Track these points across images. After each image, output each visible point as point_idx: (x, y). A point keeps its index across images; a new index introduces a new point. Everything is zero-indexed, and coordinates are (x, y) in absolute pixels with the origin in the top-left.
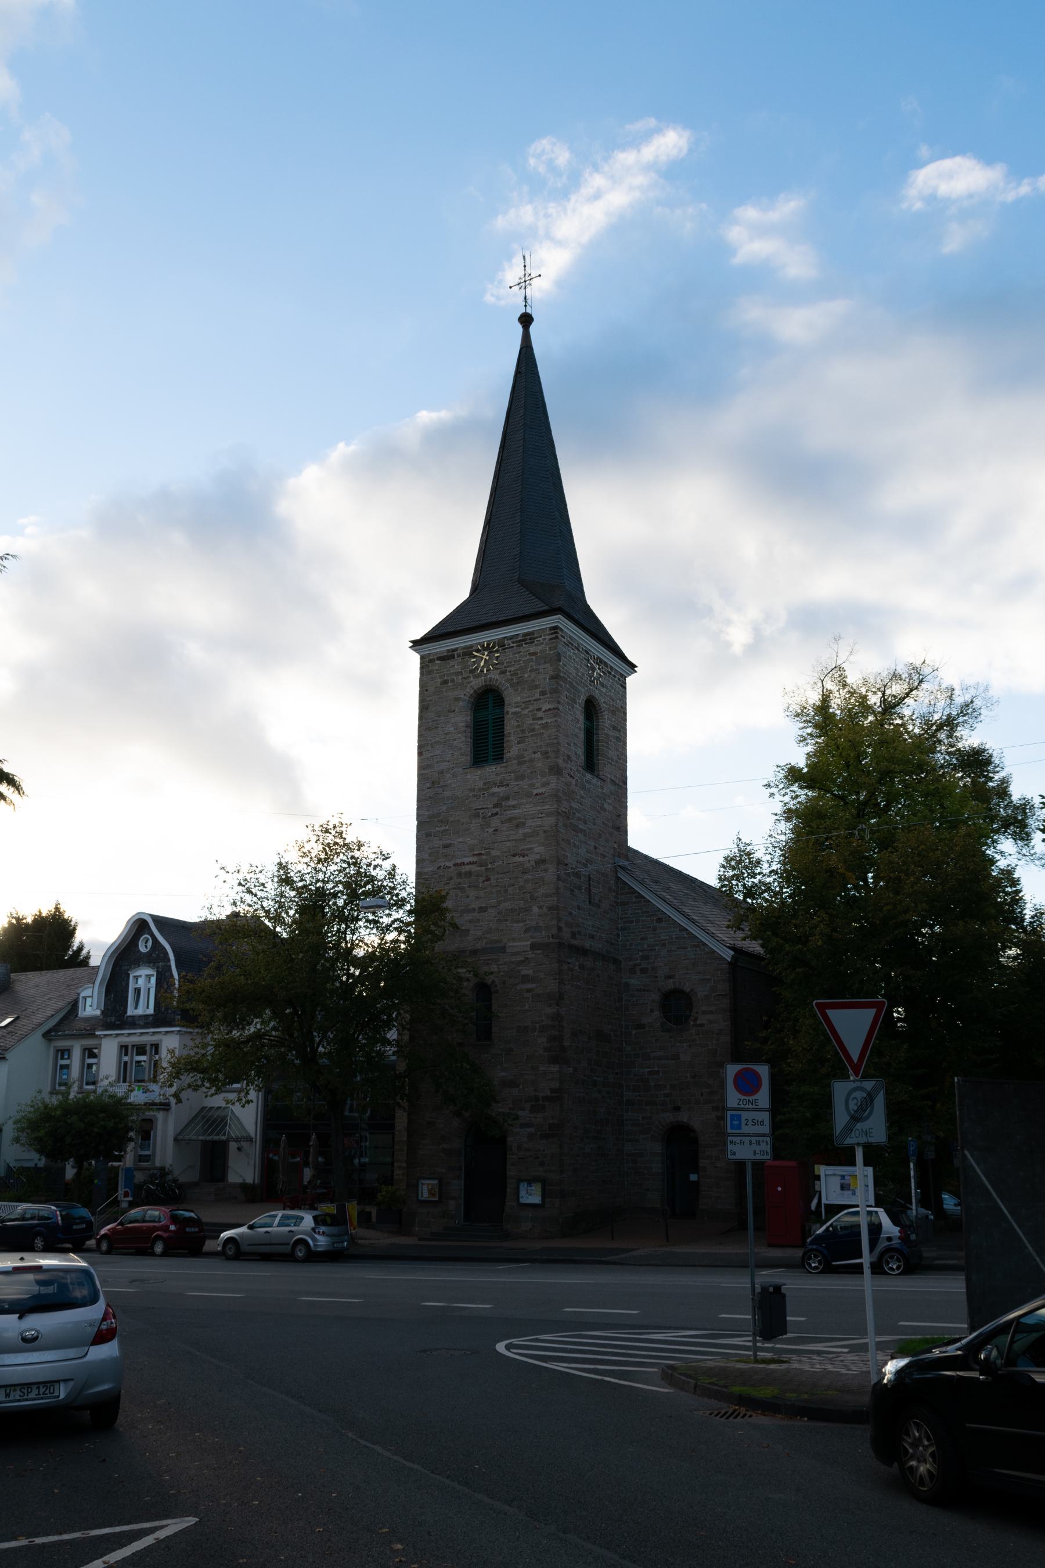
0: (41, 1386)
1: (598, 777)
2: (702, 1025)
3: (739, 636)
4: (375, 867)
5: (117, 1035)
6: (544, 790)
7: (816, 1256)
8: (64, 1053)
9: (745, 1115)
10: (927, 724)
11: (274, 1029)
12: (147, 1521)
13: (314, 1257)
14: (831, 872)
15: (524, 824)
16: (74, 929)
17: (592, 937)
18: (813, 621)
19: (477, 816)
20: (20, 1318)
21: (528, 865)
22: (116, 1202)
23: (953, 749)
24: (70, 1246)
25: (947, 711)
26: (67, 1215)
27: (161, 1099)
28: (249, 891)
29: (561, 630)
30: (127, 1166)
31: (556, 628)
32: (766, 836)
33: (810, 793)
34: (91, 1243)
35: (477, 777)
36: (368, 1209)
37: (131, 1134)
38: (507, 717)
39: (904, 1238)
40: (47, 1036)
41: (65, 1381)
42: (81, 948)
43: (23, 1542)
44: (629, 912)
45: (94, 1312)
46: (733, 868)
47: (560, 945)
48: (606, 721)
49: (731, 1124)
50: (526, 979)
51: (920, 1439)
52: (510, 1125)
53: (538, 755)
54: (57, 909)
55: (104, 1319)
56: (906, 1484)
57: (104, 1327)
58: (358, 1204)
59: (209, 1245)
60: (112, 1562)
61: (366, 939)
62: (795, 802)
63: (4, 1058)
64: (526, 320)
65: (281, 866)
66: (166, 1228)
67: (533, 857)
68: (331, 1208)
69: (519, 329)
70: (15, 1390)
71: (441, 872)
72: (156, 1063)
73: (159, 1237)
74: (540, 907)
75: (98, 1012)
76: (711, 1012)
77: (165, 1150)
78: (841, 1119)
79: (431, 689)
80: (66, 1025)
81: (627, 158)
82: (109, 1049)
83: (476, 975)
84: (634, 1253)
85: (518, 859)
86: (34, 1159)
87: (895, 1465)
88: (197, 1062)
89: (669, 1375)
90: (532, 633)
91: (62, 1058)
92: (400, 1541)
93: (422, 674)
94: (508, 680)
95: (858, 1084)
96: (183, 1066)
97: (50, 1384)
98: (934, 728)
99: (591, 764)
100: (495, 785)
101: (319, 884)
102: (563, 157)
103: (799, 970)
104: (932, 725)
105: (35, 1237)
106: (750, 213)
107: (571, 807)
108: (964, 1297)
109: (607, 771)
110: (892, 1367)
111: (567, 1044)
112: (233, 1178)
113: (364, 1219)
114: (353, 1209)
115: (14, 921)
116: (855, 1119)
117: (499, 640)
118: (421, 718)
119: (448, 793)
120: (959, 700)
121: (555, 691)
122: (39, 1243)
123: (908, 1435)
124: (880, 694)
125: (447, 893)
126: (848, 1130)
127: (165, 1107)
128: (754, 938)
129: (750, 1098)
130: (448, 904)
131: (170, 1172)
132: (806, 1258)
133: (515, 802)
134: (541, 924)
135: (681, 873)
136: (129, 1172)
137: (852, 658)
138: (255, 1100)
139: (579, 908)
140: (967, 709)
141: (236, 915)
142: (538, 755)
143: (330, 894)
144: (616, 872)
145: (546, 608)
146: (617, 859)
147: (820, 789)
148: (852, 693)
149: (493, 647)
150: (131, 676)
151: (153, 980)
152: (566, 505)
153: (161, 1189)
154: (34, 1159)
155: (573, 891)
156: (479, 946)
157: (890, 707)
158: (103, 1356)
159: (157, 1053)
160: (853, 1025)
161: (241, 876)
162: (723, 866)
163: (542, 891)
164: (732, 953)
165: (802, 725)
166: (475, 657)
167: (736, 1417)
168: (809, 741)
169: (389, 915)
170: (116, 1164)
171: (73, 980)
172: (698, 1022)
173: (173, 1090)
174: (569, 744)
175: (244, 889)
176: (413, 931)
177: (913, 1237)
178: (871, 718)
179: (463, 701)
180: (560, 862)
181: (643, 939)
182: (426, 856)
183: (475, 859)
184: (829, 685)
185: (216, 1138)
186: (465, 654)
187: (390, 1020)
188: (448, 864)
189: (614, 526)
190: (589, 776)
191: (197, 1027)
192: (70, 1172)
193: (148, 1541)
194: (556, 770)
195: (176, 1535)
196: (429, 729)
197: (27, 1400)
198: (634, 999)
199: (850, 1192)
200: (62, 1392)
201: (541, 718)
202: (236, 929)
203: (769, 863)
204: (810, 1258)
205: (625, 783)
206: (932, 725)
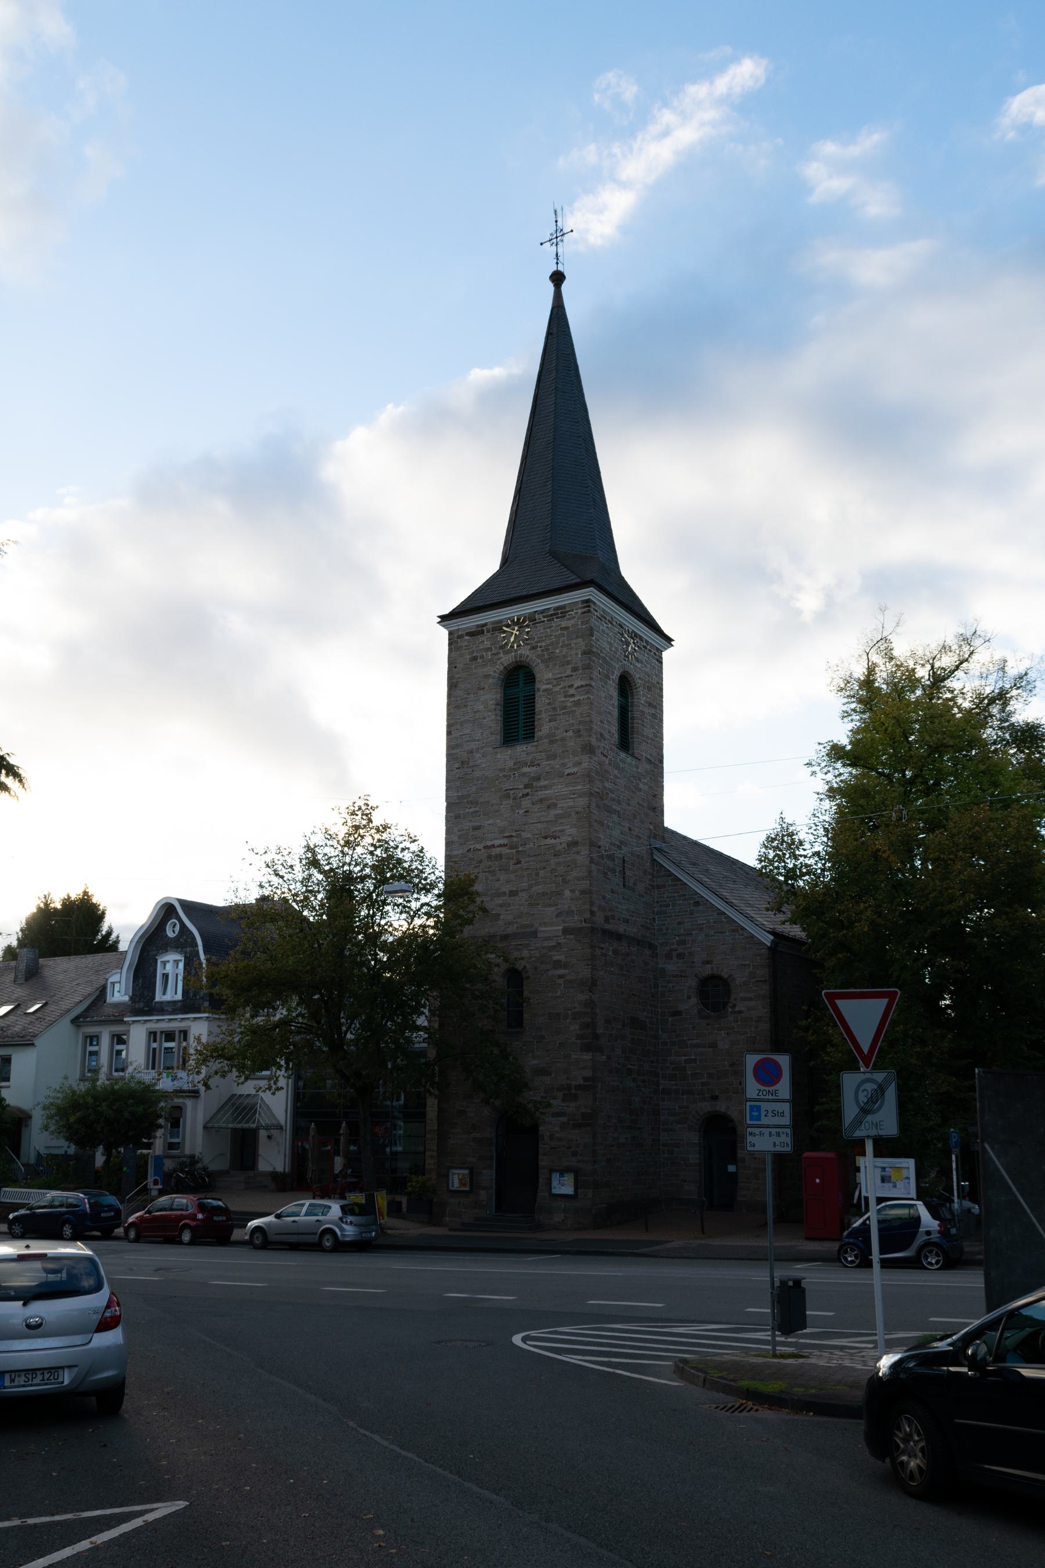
0: (46, 1372)
1: (633, 755)
2: (741, 1012)
3: (809, 603)
4: (403, 850)
6: (575, 770)
7: (852, 1250)
8: (93, 1039)
9: (764, 1106)
10: (980, 698)
11: (300, 1015)
12: (138, 1504)
13: (341, 1247)
14: (876, 855)
15: (555, 805)
16: (103, 913)
17: (627, 921)
18: (888, 586)
19: (508, 797)
20: (24, 1305)
22: (145, 1190)
23: (1007, 724)
24: (98, 1234)
25: (1000, 684)
26: (96, 1202)
27: (190, 1087)
29: (594, 603)
30: (157, 1153)
31: (588, 601)
32: (810, 815)
33: (854, 772)
34: (119, 1231)
35: (506, 757)
36: (398, 1198)
37: (161, 1121)
39: (944, 1232)
40: (75, 1021)
41: (70, 1367)
42: (109, 933)
43: (16, 1522)
44: (666, 895)
45: (99, 1300)
46: (776, 848)
47: (593, 930)
48: (641, 697)
49: (751, 1115)
50: (558, 965)
51: (910, 1435)
52: (542, 1113)
53: (570, 733)
54: (85, 893)
55: (108, 1307)
56: (897, 1479)
57: (108, 1314)
59: (237, 1234)
60: (99, 1542)
61: (396, 922)
62: (838, 779)
63: (33, 1044)
64: (558, 278)
65: (308, 848)
66: (193, 1217)
67: (565, 839)
68: (359, 1198)
69: (551, 288)
70: (19, 1376)
71: (470, 855)
72: (185, 1048)
73: (186, 1226)
74: (573, 891)
75: (126, 998)
76: (750, 999)
77: (194, 1138)
78: (850, 1111)
79: (460, 666)
80: (94, 1011)
81: (698, 91)
82: (138, 1035)
83: (506, 960)
84: (668, 1246)
85: (549, 841)
86: (63, 1146)
87: (888, 1460)
88: (223, 1049)
89: (682, 1369)
90: (564, 607)
91: (91, 1044)
92: (383, 1527)
93: (450, 650)
94: (539, 656)
95: (868, 1076)
96: (213, 1052)
97: (54, 1370)
98: (986, 701)
99: (625, 743)
100: (526, 764)
101: (346, 868)
102: (630, 91)
103: (840, 956)
104: (984, 699)
105: (63, 1225)
106: (829, 148)
107: (605, 787)
108: (983, 1293)
109: (642, 749)
110: (886, 1362)
111: (600, 1031)
112: (263, 1166)
113: (395, 1210)
114: (382, 1200)
115: (42, 905)
116: (865, 1111)
117: (531, 613)
118: (450, 696)
119: (477, 774)
120: (1013, 671)
121: (588, 667)
122: (67, 1230)
123: (900, 1431)
124: (928, 667)
125: (477, 877)
126: (858, 1122)
127: (194, 1094)
128: (793, 921)
129: (771, 1089)
130: (478, 887)
131: (200, 1160)
132: (842, 1250)
133: (546, 783)
134: (573, 908)
135: (721, 855)
136: (159, 1160)
137: (898, 630)
138: (285, 1087)
139: (612, 891)
140: (1021, 681)
141: (264, 899)
142: (570, 733)
143: (357, 878)
144: (652, 854)
146: (653, 840)
147: (864, 767)
148: (898, 666)
149: (524, 621)
150: (172, 650)
151: (181, 965)
152: (599, 473)
153: (190, 1177)
154: (63, 1146)
156: (510, 930)
157: (938, 679)
158: (108, 1343)
159: (185, 1039)
160: (863, 1016)
161: (268, 858)
162: (766, 847)
163: (574, 874)
164: (772, 937)
165: (846, 700)
166: (505, 632)
167: (741, 1412)
168: (854, 717)
169: (417, 899)
170: (145, 1151)
171: (101, 965)
172: (737, 1009)
173: (202, 1076)
174: (601, 722)
175: (270, 871)
176: (442, 915)
177: (953, 1231)
178: (919, 693)
179: (493, 677)
180: (593, 844)
181: (679, 923)
182: (455, 838)
183: (505, 841)
184: (875, 658)
185: (246, 1126)
186: (494, 629)
187: (419, 1005)
188: (478, 846)
189: (651, 496)
190: (623, 755)
191: (223, 1013)
192: (100, 1160)
193: (138, 1522)
195: (165, 1517)
196: (458, 707)
197: (31, 1385)
198: (671, 985)
199: (891, 1185)
200: (67, 1378)
201: (573, 695)
202: (266, 912)
203: (813, 845)
204: (846, 1252)
205: (661, 762)
206: (984, 699)
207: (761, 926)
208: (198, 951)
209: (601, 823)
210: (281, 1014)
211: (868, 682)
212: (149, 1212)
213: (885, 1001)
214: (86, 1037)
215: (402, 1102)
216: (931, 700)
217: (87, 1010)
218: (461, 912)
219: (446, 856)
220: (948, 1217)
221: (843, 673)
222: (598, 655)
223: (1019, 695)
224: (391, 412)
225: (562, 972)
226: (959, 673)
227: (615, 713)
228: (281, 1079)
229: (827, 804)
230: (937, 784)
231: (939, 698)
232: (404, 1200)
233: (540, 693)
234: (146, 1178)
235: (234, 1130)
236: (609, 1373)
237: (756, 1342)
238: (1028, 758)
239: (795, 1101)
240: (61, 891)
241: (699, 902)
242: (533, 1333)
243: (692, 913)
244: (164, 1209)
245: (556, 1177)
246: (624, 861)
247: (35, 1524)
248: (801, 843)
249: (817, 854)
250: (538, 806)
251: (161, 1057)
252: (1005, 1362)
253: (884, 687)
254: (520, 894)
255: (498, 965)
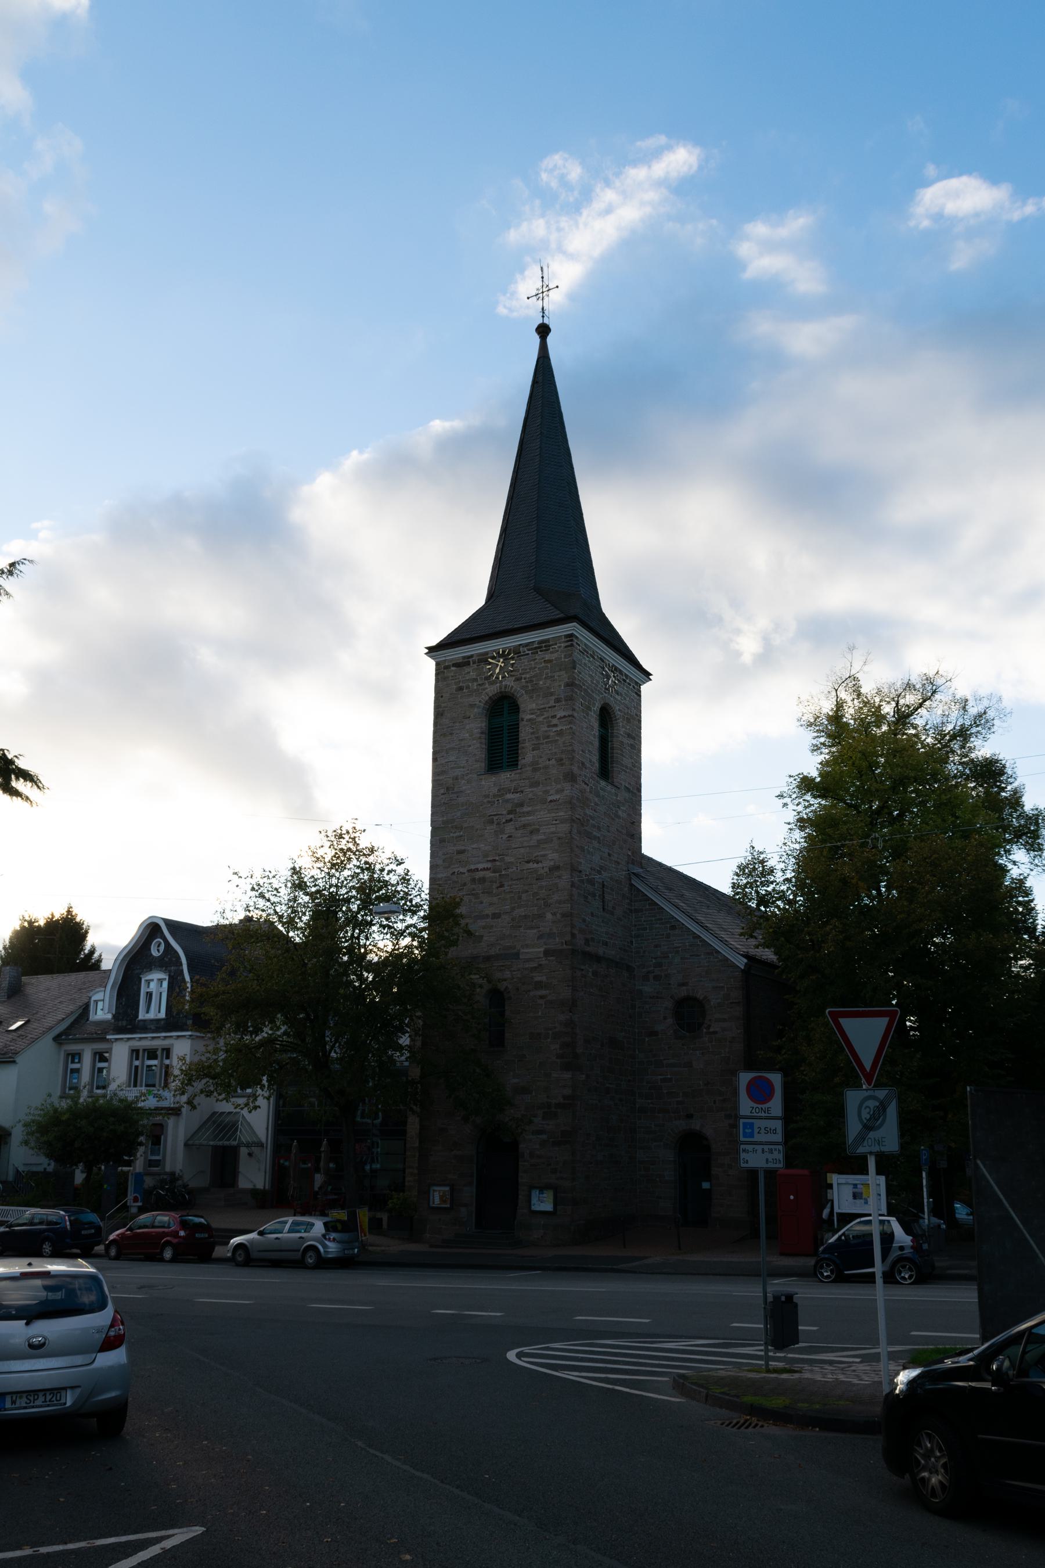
1: (612, 784)
2: (715, 1033)
3: (749, 646)
4: (389, 872)
5: (129, 1039)
6: (558, 797)
7: (828, 1265)
8: (75, 1057)
9: (757, 1123)
13: (324, 1263)
15: (538, 830)
16: (87, 932)
17: (606, 944)
19: (492, 822)
20: (27, 1324)
21: (542, 871)
22: (125, 1207)
24: (78, 1251)
26: (76, 1220)
28: (262, 896)
30: (137, 1170)
31: (571, 635)
32: (781, 844)
33: (823, 802)
34: (100, 1248)
35: (491, 783)
36: (379, 1215)
37: (142, 1139)
38: (521, 724)
39: (916, 1248)
40: (57, 1039)
41: (72, 1388)
42: (92, 952)
43: (27, 1551)
45: (102, 1319)
48: (621, 728)
49: (744, 1132)
50: (539, 985)
51: (932, 1450)
53: (553, 762)
54: (69, 912)
55: (112, 1326)
56: (917, 1495)
57: (112, 1334)
58: (370, 1210)
59: (219, 1251)
61: (380, 943)
62: (808, 810)
64: (543, 330)
65: (295, 871)
66: (175, 1234)
68: (341, 1215)
69: (537, 339)
70: (21, 1397)
73: (168, 1243)
74: (554, 914)
75: (109, 1016)
78: (853, 1128)
80: (77, 1027)
81: (638, 174)
82: (120, 1054)
83: (489, 982)
85: (531, 865)
86: (44, 1163)
87: (907, 1476)
88: (210, 1067)
89: (680, 1385)
90: (547, 641)
91: (73, 1062)
94: (522, 688)
95: (870, 1093)
96: (196, 1072)
97: (57, 1391)
98: (947, 738)
99: (605, 771)
100: (509, 791)
102: (575, 172)
104: (945, 735)
105: (43, 1243)
106: (760, 229)
107: (585, 814)
110: (903, 1377)
112: (243, 1184)
113: (375, 1225)
114: (363, 1216)
116: (868, 1127)
117: (515, 647)
120: (973, 711)
121: (570, 698)
122: (47, 1248)
123: (920, 1446)
124: (894, 704)
126: (861, 1138)
128: (766, 945)
129: (763, 1106)
130: (462, 910)
131: (181, 1177)
133: (529, 809)
134: (555, 931)
136: (139, 1178)
137: (866, 668)
139: (592, 914)
141: (248, 919)
142: (553, 762)
145: (562, 615)
146: (631, 866)
148: (866, 703)
149: (509, 654)
150: (144, 681)
151: (165, 984)
152: (581, 514)
153: (170, 1194)
154: (44, 1163)
155: (586, 897)
157: (903, 717)
159: (168, 1057)
160: (866, 1034)
164: (745, 961)
165: (816, 734)
166: (490, 663)
167: (747, 1428)
170: (125, 1169)
171: (84, 983)
172: (711, 1030)
177: (925, 1246)
178: (885, 728)
179: (479, 707)
180: (574, 869)
181: (656, 946)
182: (440, 862)
183: (489, 865)
184: (843, 695)
185: (227, 1143)
186: (480, 661)
188: (462, 870)
189: (631, 536)
190: (603, 783)
192: (79, 1177)
194: (571, 777)
196: (444, 735)
197: (33, 1407)
199: (862, 1201)
200: (69, 1399)
201: (556, 725)
202: (249, 934)
204: (822, 1267)
205: (639, 790)
206: (945, 735)
207: (735, 950)
208: (182, 971)
209: (582, 849)
210: (267, 1032)
211: (836, 718)
212: (130, 1229)
213: (886, 1020)
214: (68, 1054)
215: (378, 1121)
216: (896, 735)
217: (67, 1029)
218: (446, 934)
219: (431, 879)
220: (920, 1232)
221: (813, 709)
222: (580, 687)
223: (978, 732)
224: (355, 458)
225: (543, 992)
226: (922, 711)
227: (596, 743)
228: (260, 1099)
229: (798, 835)
230: (901, 815)
231: (904, 734)
232: (384, 1217)
233: (525, 723)
234: (126, 1196)
235: (215, 1147)
236: (609, 1389)
237: (749, 1357)
238: (987, 792)
239: (788, 1118)
240: (44, 911)
241: (675, 926)
242: (526, 1350)
243: (668, 936)
244: (145, 1227)
245: (535, 1194)
246: (603, 886)
247: (48, 1553)
248: (771, 871)
249: (788, 880)
250: (521, 831)
251: (143, 1076)
252: (1028, 1377)
253: (852, 722)
254: (503, 917)
255: (481, 986)
